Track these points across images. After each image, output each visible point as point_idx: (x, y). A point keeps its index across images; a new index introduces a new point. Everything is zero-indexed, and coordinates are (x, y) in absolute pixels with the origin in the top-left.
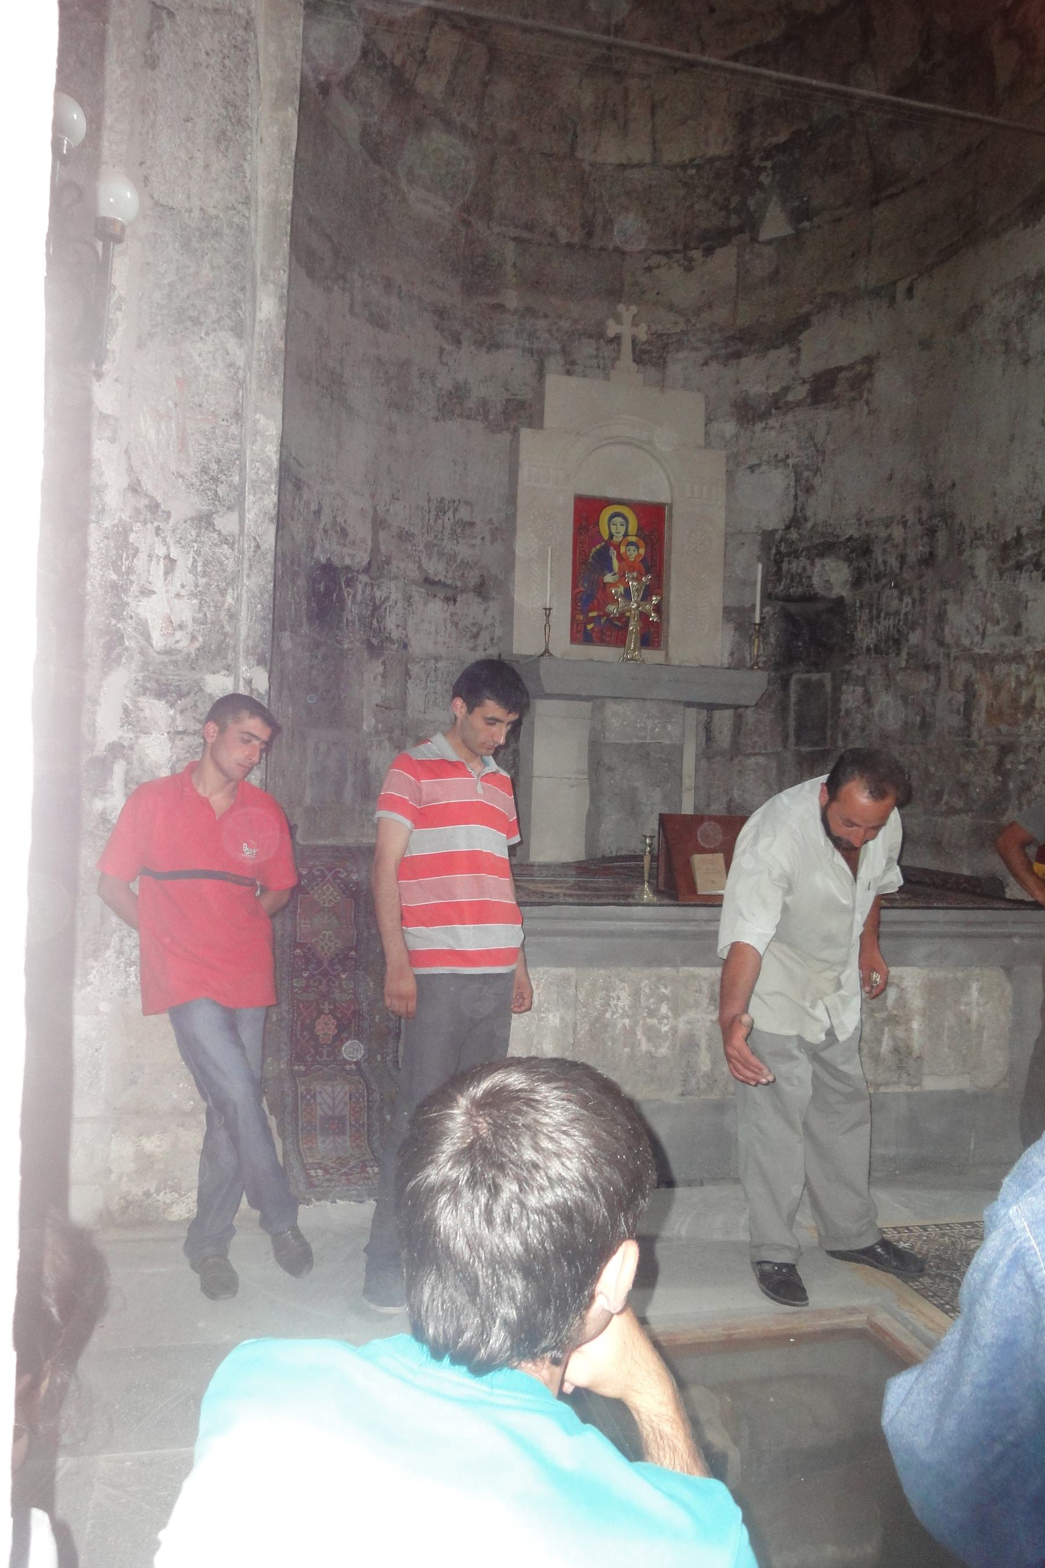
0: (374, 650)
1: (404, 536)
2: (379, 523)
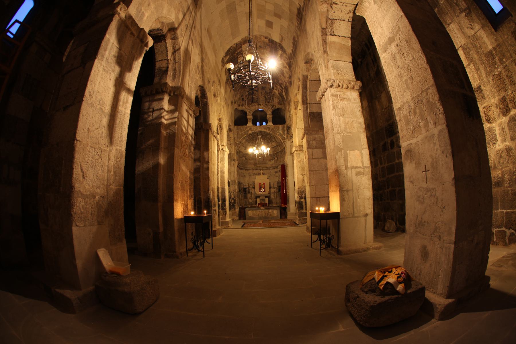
0: (249, 193)
1: (251, 185)
2: (249, 184)
